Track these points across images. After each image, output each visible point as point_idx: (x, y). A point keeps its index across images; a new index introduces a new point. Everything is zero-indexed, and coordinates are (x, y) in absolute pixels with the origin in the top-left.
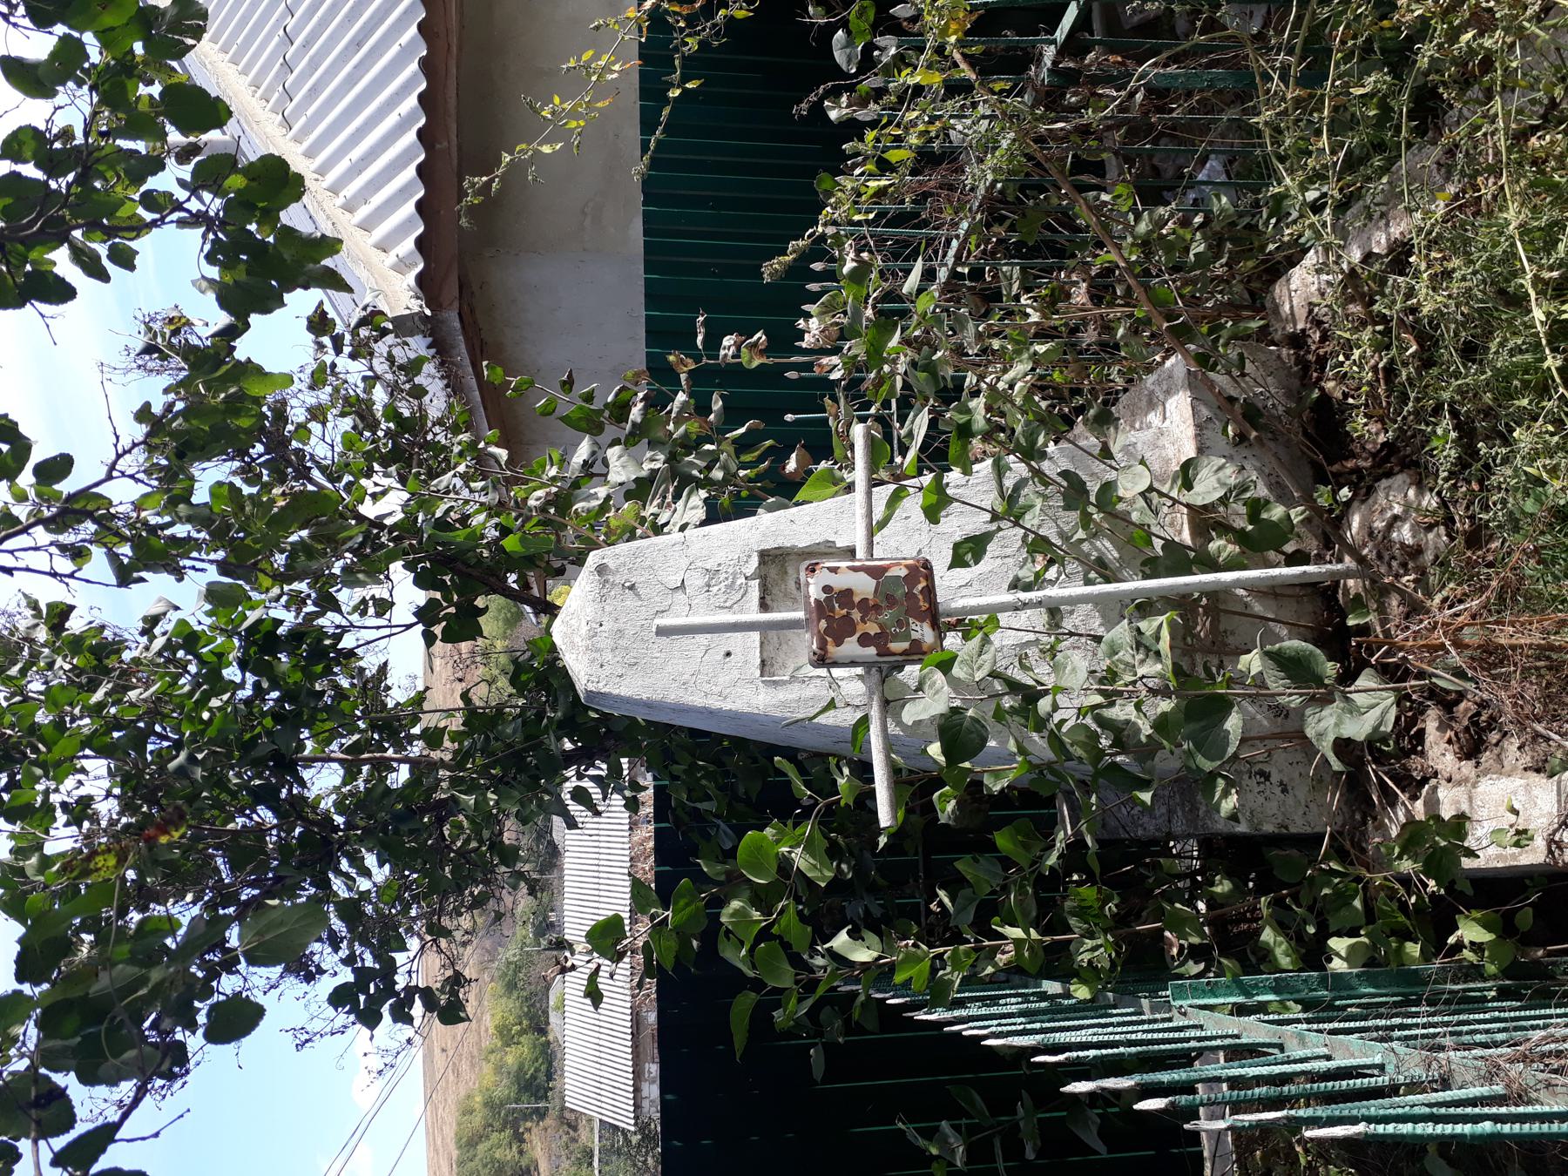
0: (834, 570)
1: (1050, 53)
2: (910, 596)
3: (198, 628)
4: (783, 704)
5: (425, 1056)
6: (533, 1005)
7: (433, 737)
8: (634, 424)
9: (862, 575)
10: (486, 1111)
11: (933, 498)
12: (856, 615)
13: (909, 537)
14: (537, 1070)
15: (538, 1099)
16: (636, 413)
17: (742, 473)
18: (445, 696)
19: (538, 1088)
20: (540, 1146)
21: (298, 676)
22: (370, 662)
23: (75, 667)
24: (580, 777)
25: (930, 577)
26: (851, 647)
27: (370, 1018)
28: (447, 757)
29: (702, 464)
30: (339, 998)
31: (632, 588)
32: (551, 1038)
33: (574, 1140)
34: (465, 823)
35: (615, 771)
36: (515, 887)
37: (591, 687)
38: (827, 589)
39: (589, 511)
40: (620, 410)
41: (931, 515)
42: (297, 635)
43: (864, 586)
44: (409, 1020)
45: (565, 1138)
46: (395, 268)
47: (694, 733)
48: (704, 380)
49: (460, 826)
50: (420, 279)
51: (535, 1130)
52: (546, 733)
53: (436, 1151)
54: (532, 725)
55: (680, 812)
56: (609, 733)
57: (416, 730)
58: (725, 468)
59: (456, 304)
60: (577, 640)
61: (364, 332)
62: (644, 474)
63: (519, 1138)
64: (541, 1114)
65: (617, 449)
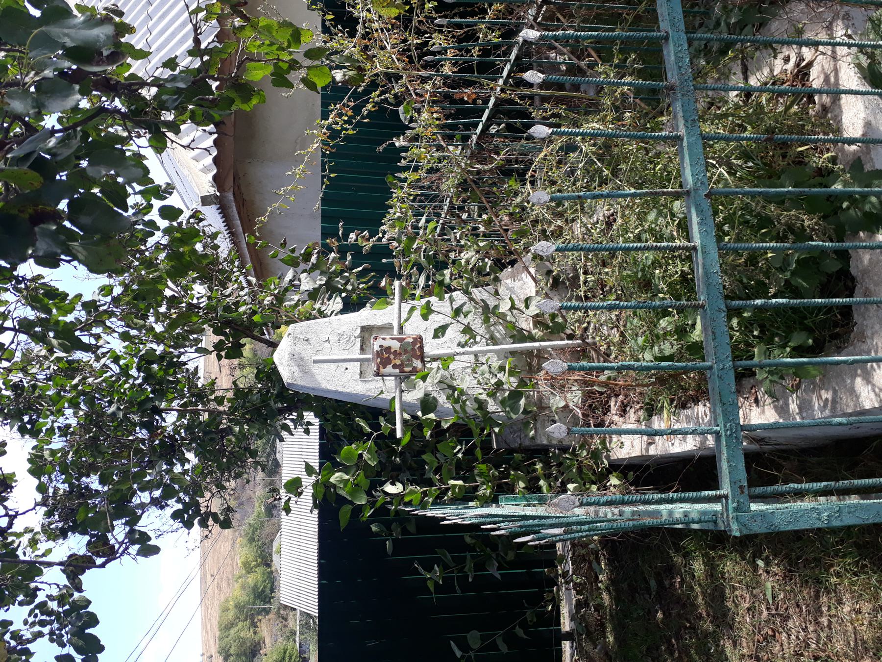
0: (384, 339)
1: (474, 137)
2: (413, 349)
3: (120, 354)
4: (369, 390)
5: (201, 579)
6: (264, 551)
7: (220, 401)
8: (313, 264)
9: (395, 341)
10: (237, 611)
11: (425, 311)
12: (392, 357)
13: (416, 327)
14: (265, 587)
15: (265, 603)
16: (314, 259)
17: (361, 286)
18: (224, 383)
19: (266, 597)
20: (267, 630)
21: (162, 373)
22: (191, 366)
23: (59, 368)
24: (285, 419)
25: (421, 342)
26: (389, 369)
27: (189, 525)
28: (226, 409)
29: (343, 282)
30: (176, 515)
31: (307, 340)
32: (273, 569)
33: (286, 626)
34: (234, 440)
35: (300, 417)
36: (255, 468)
37: (289, 381)
38: (381, 346)
39: (290, 306)
40: (307, 256)
41: (425, 317)
42: (162, 357)
43: (396, 345)
44: (207, 527)
45: (280, 625)
46: (202, 170)
47: (337, 401)
48: (342, 252)
49: (230, 441)
50: (215, 178)
51: (263, 620)
52: (272, 402)
53: (207, 632)
54: (264, 395)
55: (329, 435)
56: (298, 401)
57: (212, 397)
58: (352, 285)
59: (232, 189)
60: (284, 361)
61: (192, 220)
62: (316, 286)
63: (254, 625)
64: (267, 612)
65: (305, 274)
